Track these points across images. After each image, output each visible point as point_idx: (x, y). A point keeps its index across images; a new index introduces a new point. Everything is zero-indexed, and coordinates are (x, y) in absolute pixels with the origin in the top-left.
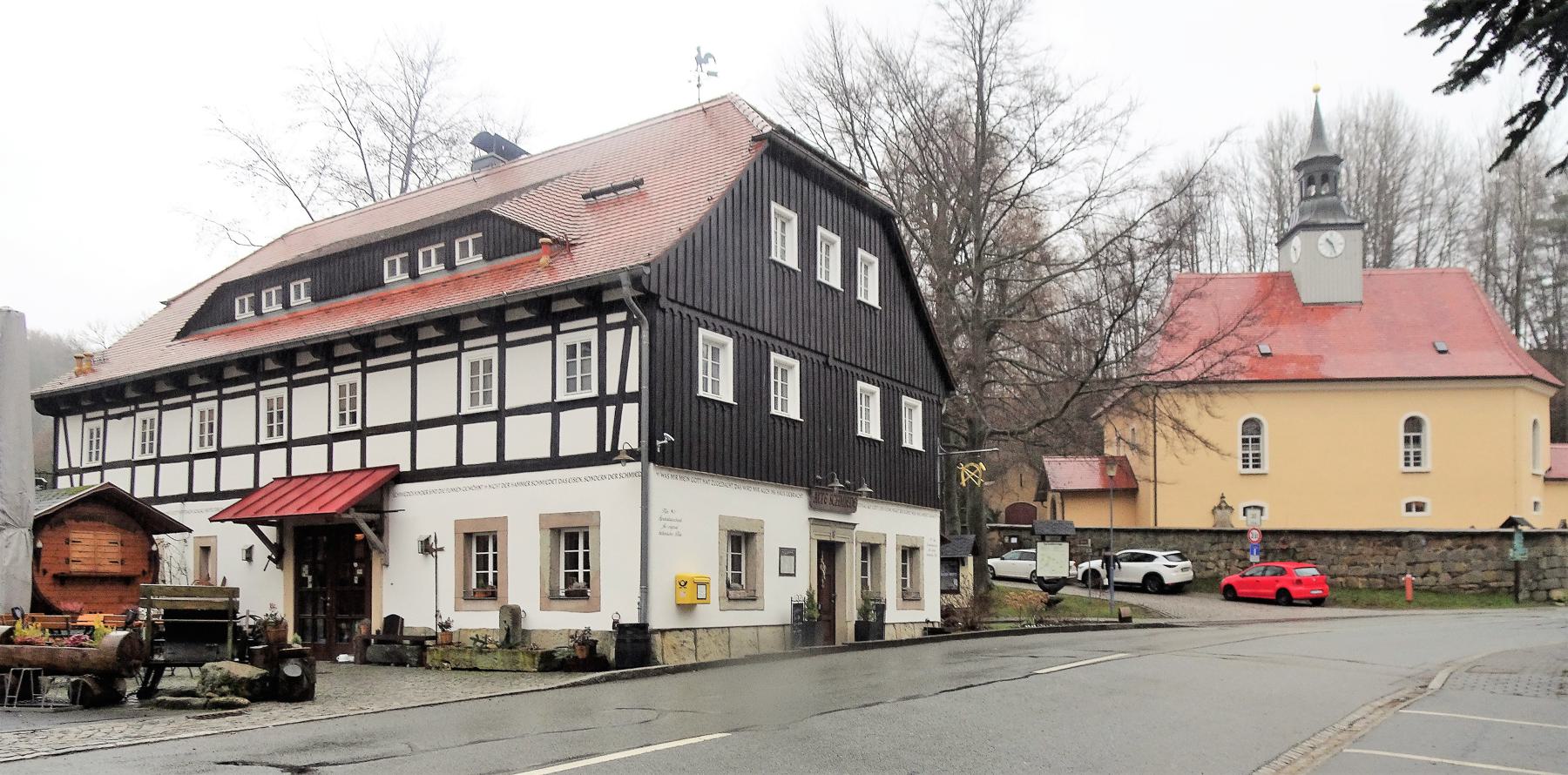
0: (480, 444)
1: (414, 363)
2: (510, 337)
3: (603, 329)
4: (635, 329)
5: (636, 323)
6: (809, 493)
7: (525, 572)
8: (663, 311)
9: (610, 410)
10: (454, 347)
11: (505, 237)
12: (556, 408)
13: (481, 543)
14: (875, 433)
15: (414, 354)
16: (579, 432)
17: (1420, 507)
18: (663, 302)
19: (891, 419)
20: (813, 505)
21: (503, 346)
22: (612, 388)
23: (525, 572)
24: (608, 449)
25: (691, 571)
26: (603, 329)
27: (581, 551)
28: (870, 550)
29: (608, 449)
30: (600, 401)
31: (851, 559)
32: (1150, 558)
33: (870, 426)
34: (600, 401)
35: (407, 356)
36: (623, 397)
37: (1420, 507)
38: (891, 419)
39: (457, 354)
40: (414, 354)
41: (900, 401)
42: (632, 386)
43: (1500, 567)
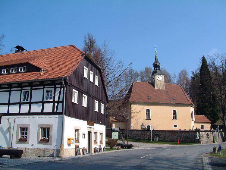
0: (25, 109)
1: (10, 91)
2: (33, 88)
3: (55, 88)
4: (62, 89)
5: (63, 87)
6: (88, 121)
7: (34, 135)
8: (68, 85)
9: (56, 104)
10: (20, 89)
11: (31, 68)
12: (43, 103)
13: (24, 130)
14: (76, 102)
15: (10, 89)
16: (48, 108)
17: (176, 126)
18: (69, 84)
19: (80, 99)
20: (88, 124)
21: (32, 89)
22: (56, 99)
23: (34, 135)
24: (55, 111)
25: (69, 137)
26: (55, 88)
27: (25, 132)
28: (95, 133)
29: (55, 111)
30: (54, 102)
31: (93, 135)
32: (130, 147)
33: (75, 100)
34: (54, 102)
35: (9, 89)
36: (58, 102)
37: (176, 126)
38: (80, 99)
39: (21, 90)
40: (10, 89)
41: (72, 90)
42: (61, 99)
43: (19, 78)
